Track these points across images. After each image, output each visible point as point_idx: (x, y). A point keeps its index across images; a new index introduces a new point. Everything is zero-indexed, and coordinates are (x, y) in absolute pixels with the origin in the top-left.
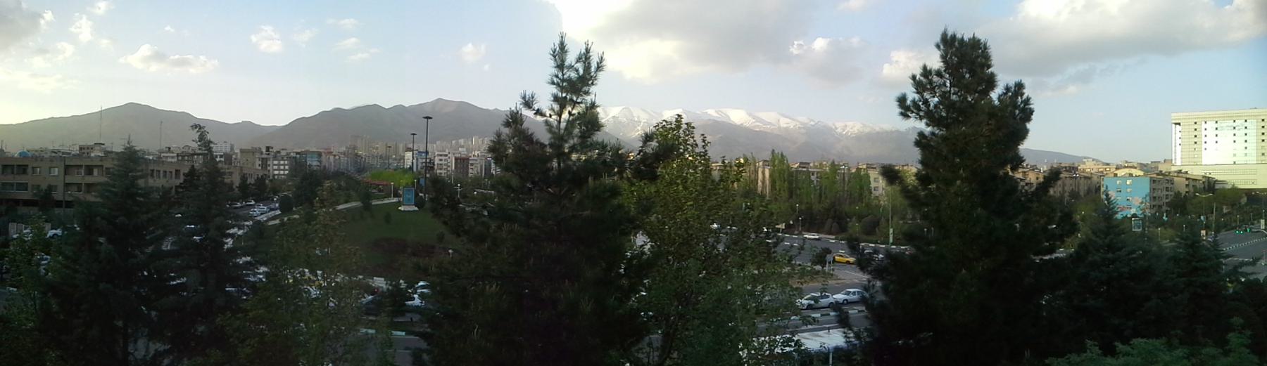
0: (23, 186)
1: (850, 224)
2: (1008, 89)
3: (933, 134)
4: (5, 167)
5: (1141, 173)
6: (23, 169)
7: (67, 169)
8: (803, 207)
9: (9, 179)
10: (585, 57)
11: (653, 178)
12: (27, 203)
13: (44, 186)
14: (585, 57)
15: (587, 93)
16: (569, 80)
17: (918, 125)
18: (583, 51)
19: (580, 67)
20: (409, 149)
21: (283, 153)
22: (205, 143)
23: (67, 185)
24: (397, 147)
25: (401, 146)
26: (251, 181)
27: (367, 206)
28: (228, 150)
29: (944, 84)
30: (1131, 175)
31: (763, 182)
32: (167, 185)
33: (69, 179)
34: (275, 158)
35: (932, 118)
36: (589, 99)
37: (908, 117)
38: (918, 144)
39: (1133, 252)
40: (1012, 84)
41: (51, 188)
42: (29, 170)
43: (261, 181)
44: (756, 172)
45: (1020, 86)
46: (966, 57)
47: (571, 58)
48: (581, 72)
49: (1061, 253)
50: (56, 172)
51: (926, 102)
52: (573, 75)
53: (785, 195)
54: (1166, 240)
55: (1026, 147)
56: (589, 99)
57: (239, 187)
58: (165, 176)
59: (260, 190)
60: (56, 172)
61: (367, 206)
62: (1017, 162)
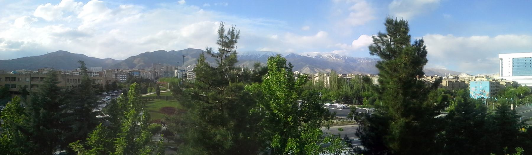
0: (14, 86)
1: (363, 101)
2: (416, 42)
3: (383, 62)
4: (6, 78)
5: (486, 80)
6: (14, 79)
7: (32, 79)
8: (344, 93)
9: (8, 83)
10: (232, 33)
11: (260, 81)
12: (16, 93)
13: (23, 86)
14: (232, 33)
15: (232, 47)
16: (225, 42)
17: (377, 58)
18: (231, 30)
19: (229, 37)
20: (176, 69)
21: (124, 71)
22: (84, 70)
23: (32, 86)
24: (171, 67)
25: (173, 68)
26: (110, 83)
27: (158, 93)
28: (101, 71)
29: (388, 40)
30: (481, 80)
31: (327, 82)
32: (75, 86)
33: (33, 83)
34: (121, 74)
35: (382, 54)
36: (233, 50)
37: (373, 54)
38: (377, 66)
39: (477, 114)
40: (418, 40)
41: (26, 87)
42: (17, 79)
43: (114, 83)
44: (324, 78)
45: (422, 41)
46: (398, 29)
47: (225, 33)
48: (230, 38)
49: (443, 115)
50: (28, 80)
51: (379, 48)
52: (227, 41)
53: (336, 87)
54: (492, 110)
55: (426, 68)
56: (233, 50)
57: (105, 86)
58: (74, 82)
59: (113, 87)
60: (28, 80)
61: (158, 93)
62: (421, 74)
